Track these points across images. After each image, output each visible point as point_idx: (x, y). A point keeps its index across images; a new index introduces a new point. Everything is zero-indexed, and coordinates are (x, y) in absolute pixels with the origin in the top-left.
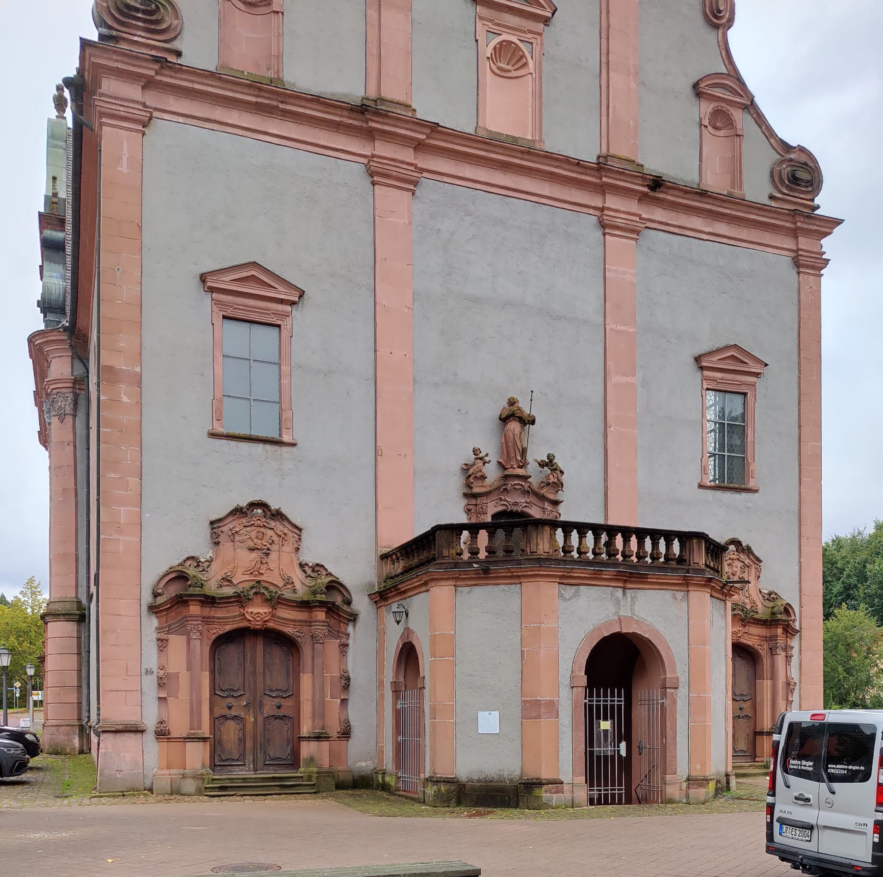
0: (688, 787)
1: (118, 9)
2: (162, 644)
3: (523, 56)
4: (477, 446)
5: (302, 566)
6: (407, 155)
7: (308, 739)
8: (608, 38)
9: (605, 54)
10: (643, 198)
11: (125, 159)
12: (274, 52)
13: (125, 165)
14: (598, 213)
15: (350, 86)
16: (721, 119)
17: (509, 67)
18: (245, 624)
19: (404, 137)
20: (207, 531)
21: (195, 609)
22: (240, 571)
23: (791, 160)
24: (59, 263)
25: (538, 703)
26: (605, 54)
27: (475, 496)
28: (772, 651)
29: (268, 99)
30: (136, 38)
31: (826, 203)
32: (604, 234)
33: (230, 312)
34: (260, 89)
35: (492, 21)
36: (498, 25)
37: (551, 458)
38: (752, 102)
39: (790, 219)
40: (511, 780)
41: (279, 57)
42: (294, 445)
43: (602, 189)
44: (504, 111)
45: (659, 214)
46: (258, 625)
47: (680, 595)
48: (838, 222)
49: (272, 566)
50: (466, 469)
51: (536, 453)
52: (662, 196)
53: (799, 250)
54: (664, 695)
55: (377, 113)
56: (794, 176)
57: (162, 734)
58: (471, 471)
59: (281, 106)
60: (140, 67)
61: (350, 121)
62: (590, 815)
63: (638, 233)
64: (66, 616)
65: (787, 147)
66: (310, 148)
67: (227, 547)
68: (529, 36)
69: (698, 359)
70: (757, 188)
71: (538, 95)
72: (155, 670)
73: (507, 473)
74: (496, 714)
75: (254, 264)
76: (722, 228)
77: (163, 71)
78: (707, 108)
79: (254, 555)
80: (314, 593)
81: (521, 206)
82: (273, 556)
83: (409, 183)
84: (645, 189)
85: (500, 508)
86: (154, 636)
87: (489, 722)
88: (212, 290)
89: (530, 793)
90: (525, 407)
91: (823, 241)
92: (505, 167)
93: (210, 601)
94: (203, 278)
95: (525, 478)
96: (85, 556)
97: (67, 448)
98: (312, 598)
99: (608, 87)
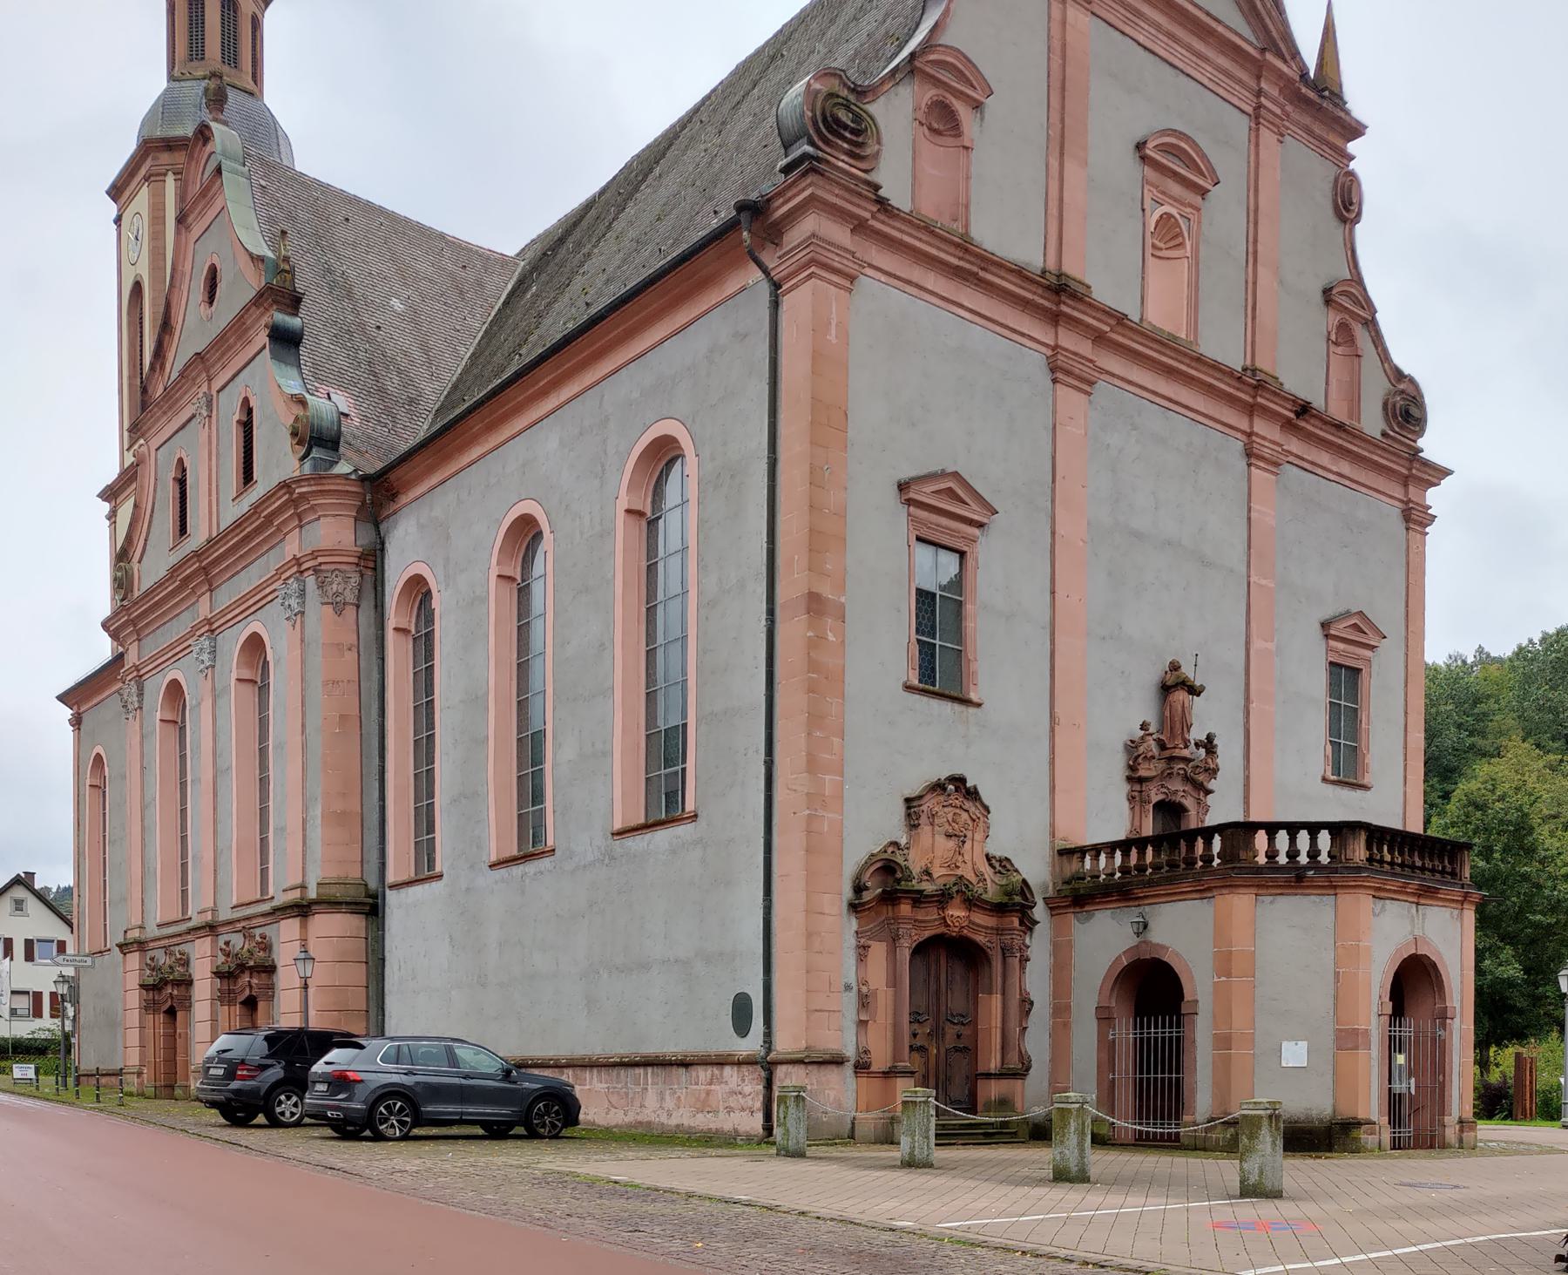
0: (1461, 1131)
1: (825, 120)
2: (862, 951)
3: (1181, 234)
4: (1148, 720)
5: (988, 858)
6: (1085, 348)
7: (1001, 1075)
8: (1256, 223)
9: (1253, 241)
10: (1288, 426)
11: (834, 323)
12: (962, 200)
13: (833, 332)
14: (1244, 438)
15: (1028, 251)
16: (1344, 335)
17: (1161, 245)
18: (943, 930)
19: (1088, 326)
20: (901, 809)
21: (905, 909)
22: (937, 862)
23: (1403, 392)
24: (292, 365)
25: (1355, 1032)
26: (1253, 241)
27: (1141, 780)
28: (1006, 952)
29: (970, 266)
30: (840, 164)
31: (1432, 445)
32: (1249, 465)
33: (925, 534)
34: (966, 250)
35: (1157, 187)
36: (1163, 193)
37: (1210, 738)
38: (1374, 318)
39: (1407, 464)
40: (1321, 1121)
41: (967, 207)
42: (979, 705)
43: (1251, 410)
44: (1163, 311)
45: (1295, 445)
46: (954, 932)
47: (1456, 912)
48: (1446, 473)
49: (967, 857)
50: (1132, 747)
51: (1197, 734)
52: (1302, 424)
53: (1410, 501)
54: (1444, 1026)
55: (1074, 296)
56: (1407, 412)
57: (862, 1067)
58: (1141, 749)
59: (982, 274)
60: (859, 206)
61: (1041, 301)
62: (1391, 1157)
63: (1277, 465)
64: (353, 906)
65: (1399, 375)
66: (998, 329)
67: (925, 829)
68: (1189, 210)
69: (1325, 625)
70: (1372, 422)
71: (1194, 286)
72: (854, 985)
73: (1167, 754)
74: (1303, 1045)
75: (956, 475)
76: (1345, 467)
77: (879, 216)
78: (1334, 318)
79: (952, 844)
80: (1009, 894)
81: (1179, 422)
82: (968, 845)
83: (1085, 384)
84: (1292, 415)
85: (1161, 797)
86: (853, 942)
87: (1295, 1054)
88: (910, 502)
89: (1347, 1135)
90: (1187, 671)
91: (1431, 492)
92: (1170, 372)
93: (918, 899)
94: (903, 487)
95: (1187, 760)
96: (376, 816)
97: (347, 653)
98: (1005, 900)
99: (1255, 283)
